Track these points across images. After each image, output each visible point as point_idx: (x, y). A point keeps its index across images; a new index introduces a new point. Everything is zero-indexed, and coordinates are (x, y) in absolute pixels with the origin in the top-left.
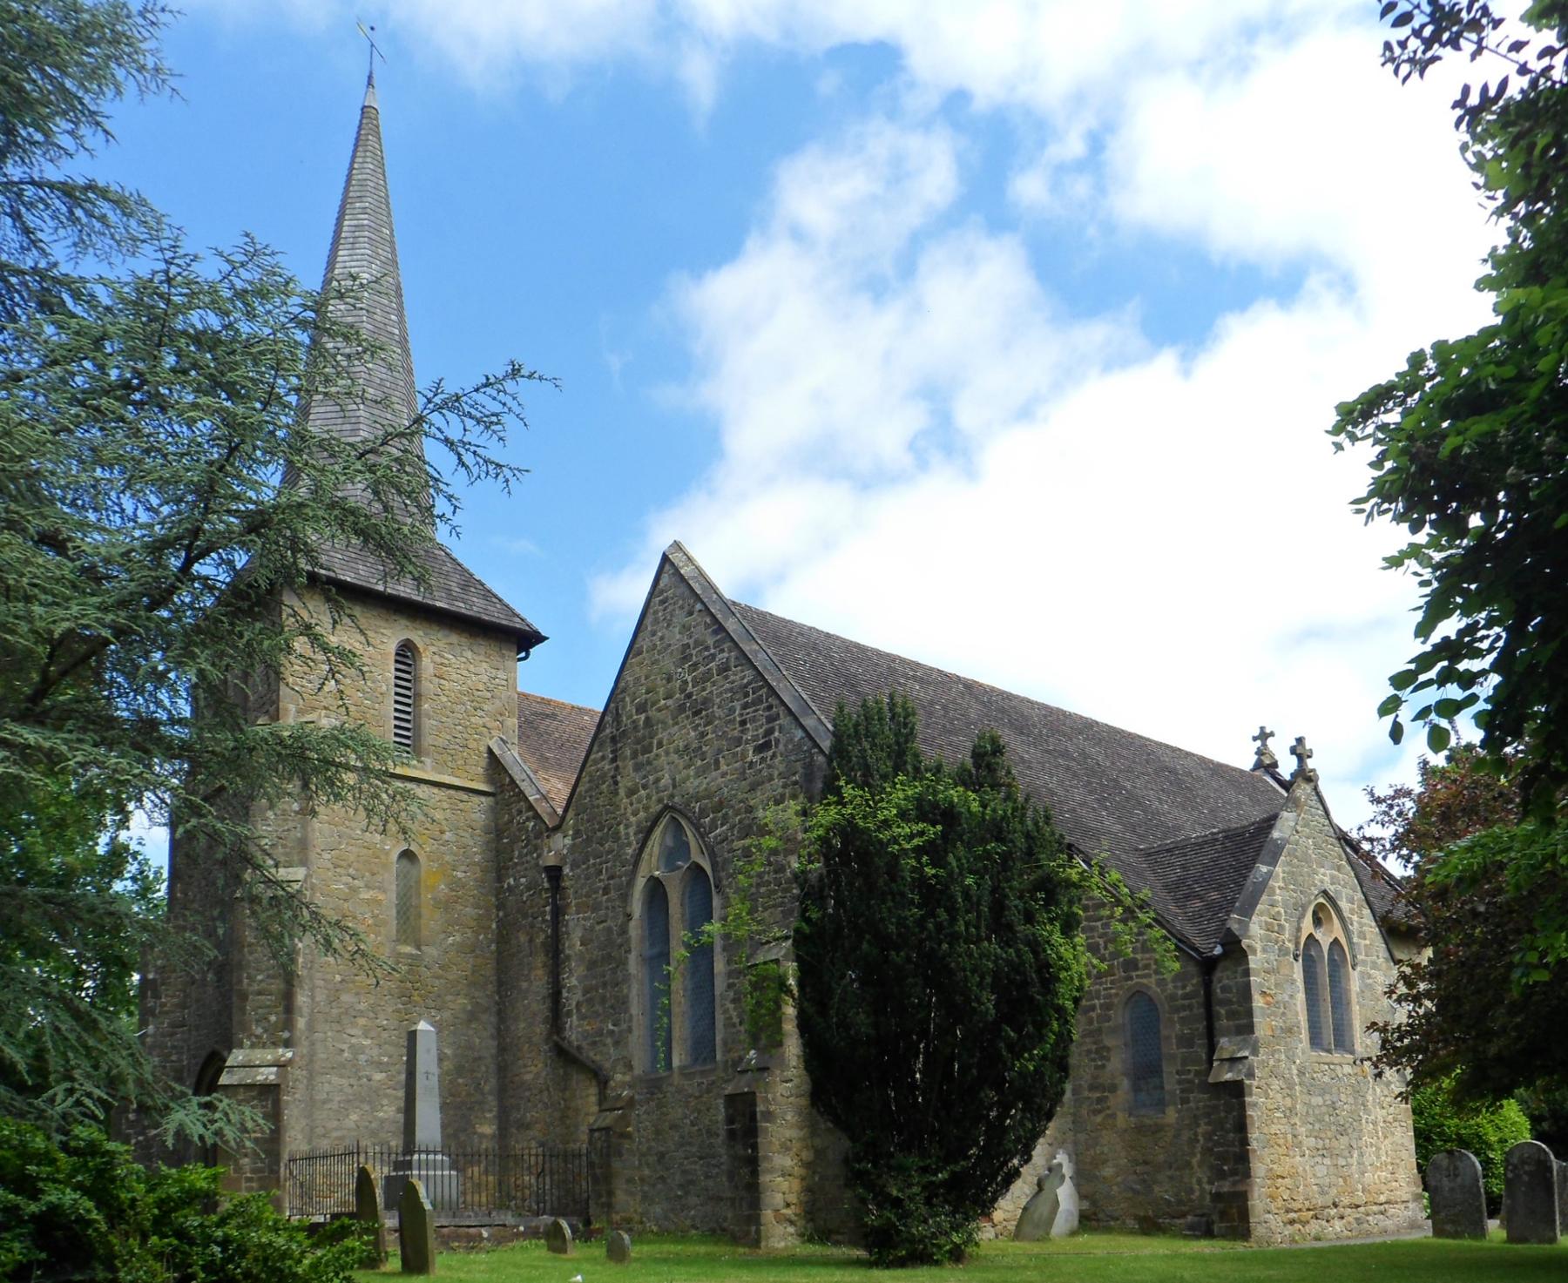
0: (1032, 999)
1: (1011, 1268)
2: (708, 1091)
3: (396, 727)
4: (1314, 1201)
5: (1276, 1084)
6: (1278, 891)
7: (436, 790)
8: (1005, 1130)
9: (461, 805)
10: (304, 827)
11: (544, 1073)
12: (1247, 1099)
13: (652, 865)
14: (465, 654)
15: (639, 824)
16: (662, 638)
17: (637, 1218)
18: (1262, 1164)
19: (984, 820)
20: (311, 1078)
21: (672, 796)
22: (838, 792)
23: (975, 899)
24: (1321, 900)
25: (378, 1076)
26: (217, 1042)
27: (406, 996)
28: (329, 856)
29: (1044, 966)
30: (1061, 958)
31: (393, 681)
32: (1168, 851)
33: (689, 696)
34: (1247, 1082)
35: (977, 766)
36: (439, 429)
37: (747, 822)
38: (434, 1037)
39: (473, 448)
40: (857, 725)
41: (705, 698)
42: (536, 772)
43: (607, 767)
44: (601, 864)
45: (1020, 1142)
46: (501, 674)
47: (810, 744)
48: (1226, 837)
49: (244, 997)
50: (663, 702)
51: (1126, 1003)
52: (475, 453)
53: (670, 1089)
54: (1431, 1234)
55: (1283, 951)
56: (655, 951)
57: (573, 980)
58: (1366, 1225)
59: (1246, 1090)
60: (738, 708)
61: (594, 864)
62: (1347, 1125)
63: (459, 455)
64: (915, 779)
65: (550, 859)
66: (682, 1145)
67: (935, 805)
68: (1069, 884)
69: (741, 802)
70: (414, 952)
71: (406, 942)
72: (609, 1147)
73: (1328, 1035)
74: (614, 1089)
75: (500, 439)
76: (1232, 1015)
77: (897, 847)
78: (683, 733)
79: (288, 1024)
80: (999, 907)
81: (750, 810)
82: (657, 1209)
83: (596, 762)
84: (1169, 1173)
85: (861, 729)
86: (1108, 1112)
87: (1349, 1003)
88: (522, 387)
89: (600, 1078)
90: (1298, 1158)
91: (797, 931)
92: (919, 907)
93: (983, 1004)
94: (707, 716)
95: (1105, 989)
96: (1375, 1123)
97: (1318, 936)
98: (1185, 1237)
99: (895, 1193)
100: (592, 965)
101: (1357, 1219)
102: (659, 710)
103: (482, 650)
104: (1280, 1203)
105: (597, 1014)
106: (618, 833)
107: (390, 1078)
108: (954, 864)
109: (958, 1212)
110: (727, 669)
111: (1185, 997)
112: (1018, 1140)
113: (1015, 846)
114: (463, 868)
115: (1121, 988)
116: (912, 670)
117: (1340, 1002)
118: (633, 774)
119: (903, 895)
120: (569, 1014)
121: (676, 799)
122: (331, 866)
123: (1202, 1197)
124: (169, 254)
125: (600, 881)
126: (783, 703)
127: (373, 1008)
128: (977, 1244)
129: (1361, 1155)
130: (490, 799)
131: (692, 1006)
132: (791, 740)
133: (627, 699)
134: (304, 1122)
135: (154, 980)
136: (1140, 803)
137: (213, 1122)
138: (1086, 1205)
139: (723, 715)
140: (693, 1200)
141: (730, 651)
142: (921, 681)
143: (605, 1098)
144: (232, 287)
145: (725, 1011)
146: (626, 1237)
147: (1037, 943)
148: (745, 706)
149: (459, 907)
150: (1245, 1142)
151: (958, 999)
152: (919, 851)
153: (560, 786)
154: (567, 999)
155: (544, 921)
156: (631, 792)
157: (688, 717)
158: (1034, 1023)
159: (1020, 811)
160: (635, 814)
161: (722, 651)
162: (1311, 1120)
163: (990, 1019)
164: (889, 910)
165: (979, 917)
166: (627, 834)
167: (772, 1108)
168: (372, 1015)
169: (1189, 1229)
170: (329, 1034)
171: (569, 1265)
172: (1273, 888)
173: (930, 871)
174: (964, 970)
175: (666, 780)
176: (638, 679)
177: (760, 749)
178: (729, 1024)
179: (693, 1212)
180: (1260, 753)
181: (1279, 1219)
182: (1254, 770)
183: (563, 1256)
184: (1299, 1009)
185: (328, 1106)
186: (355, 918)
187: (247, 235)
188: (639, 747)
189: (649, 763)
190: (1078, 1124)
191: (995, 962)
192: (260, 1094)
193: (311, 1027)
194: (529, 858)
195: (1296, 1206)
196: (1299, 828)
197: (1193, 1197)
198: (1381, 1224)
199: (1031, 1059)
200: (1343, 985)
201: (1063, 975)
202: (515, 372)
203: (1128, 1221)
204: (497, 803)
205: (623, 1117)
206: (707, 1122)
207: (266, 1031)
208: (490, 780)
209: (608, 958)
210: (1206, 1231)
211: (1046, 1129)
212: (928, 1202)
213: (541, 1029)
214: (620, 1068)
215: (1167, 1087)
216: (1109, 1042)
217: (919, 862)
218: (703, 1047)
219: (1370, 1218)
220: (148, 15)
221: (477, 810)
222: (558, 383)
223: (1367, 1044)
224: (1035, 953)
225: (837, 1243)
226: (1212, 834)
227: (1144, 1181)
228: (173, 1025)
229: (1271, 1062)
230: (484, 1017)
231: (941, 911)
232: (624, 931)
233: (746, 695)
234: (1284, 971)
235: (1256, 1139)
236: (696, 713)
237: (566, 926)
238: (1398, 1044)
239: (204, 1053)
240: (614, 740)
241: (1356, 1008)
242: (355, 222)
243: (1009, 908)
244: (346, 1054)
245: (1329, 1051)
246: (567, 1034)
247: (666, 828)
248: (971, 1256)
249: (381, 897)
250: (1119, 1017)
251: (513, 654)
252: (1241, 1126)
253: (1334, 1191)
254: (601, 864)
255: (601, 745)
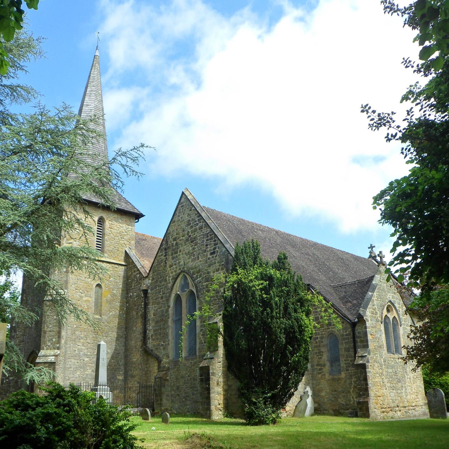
0: (296, 337)
1: (291, 426)
2: (194, 365)
3: (97, 244)
4: (390, 405)
5: (376, 365)
6: (375, 301)
7: (108, 264)
8: (289, 380)
9: (116, 269)
10: (67, 277)
11: (140, 359)
12: (367, 370)
13: (177, 290)
14: (119, 221)
15: (173, 276)
16: (181, 218)
17: (170, 409)
18: (372, 392)
19: (281, 280)
20: (65, 360)
21: (184, 268)
22: (236, 270)
23: (279, 305)
24: (389, 304)
25: (86, 359)
26: (34, 348)
27: (96, 333)
28: (74, 286)
29: (300, 326)
30: (305, 324)
31: (96, 229)
32: (340, 286)
33: (190, 236)
34: (367, 364)
35: (279, 262)
36: (120, 161)
37: (207, 277)
38: (106, 345)
39: (129, 167)
40: (242, 249)
41: (195, 237)
42: (140, 258)
43: (163, 258)
44: (160, 289)
45: (294, 384)
46: (130, 227)
47: (227, 252)
48: (358, 283)
49: (45, 332)
50: (181, 238)
51: (328, 337)
52: (130, 168)
53: (182, 364)
54: (429, 417)
55: (377, 321)
56: (178, 318)
57: (151, 327)
58: (408, 414)
59: (367, 367)
60: (205, 240)
61: (158, 289)
62: (401, 379)
63: (125, 169)
64: (260, 267)
65: (144, 287)
66: (185, 383)
67: (266, 275)
68: (307, 300)
69: (206, 270)
70: (100, 317)
71: (97, 314)
72: (161, 384)
73: (393, 349)
74: (163, 364)
75: (138, 164)
76: (362, 341)
77: (254, 288)
78: (188, 248)
79: (59, 342)
80: (286, 308)
81: (208, 273)
82: (177, 406)
83: (160, 256)
84: (343, 395)
85: (244, 251)
86: (323, 373)
87: (400, 338)
88: (144, 149)
89: (159, 361)
90: (385, 390)
91: (224, 314)
92: (262, 307)
93: (281, 338)
94: (195, 242)
95: (321, 332)
96: (410, 378)
97: (389, 315)
98: (349, 417)
99: (254, 400)
100: (157, 322)
101: (405, 411)
102: (180, 240)
103: (124, 219)
104: (379, 405)
105: (158, 339)
106: (166, 279)
107: (90, 360)
108: (272, 294)
109: (274, 407)
110: (202, 228)
111: (347, 335)
112: (293, 383)
113: (291, 288)
114: (116, 290)
115: (326, 332)
116: (259, 227)
117: (397, 338)
118: (171, 261)
119: (256, 303)
120: (149, 338)
121: (185, 269)
122: (74, 289)
123: (354, 403)
124: (42, 110)
125: (160, 295)
126: (219, 239)
127: (86, 337)
128: (280, 418)
129: (406, 389)
130: (126, 267)
131: (189, 336)
132: (222, 251)
133: (170, 236)
134: (62, 375)
135: (15, 326)
136: (331, 270)
137: (41, 375)
138: (316, 405)
139: (200, 243)
140: (188, 402)
141: (203, 222)
142: (262, 231)
143: (160, 368)
144: (59, 117)
145: (200, 338)
146: (168, 414)
147: (298, 319)
148: (207, 240)
149: (114, 303)
150: (367, 384)
151: (274, 337)
152: (261, 290)
153: (147, 263)
154: (148, 333)
155: (141, 307)
156: (171, 266)
157: (189, 243)
158: (297, 345)
159: (292, 277)
160: (172, 273)
161: (200, 222)
162: (388, 377)
163: (284, 343)
164: (252, 308)
165: (280, 311)
166: (169, 280)
167: (215, 371)
168: (85, 339)
169: (350, 414)
170: (71, 345)
171: (150, 424)
172: (373, 300)
173: (265, 296)
174: (275, 327)
175: (182, 263)
176: (174, 230)
177: (212, 254)
178: (201, 343)
179: (188, 407)
180: (370, 252)
181: (379, 411)
182: (369, 258)
183: (147, 421)
184: (383, 340)
185: (70, 370)
186: (81, 306)
187: (63, 103)
188: (174, 252)
189: (177, 257)
190: (313, 378)
191: (285, 325)
192: (49, 366)
193: (66, 343)
194: (137, 286)
195: (385, 406)
196: (381, 280)
197: (351, 403)
198: (414, 413)
199: (297, 357)
200: (397, 332)
201: (306, 329)
202: (142, 146)
203: (330, 411)
204: (127, 268)
205: (166, 373)
206: (193, 376)
207: (52, 344)
208: (125, 261)
209: (162, 320)
210: (355, 415)
211: (302, 379)
212: (265, 403)
213: (139, 344)
214: (165, 357)
215: (342, 365)
216: (323, 349)
217: (261, 293)
218: (192, 351)
219: (410, 411)
220: (39, 40)
221: (121, 271)
222: (155, 148)
223: (404, 352)
224: (298, 322)
225: (235, 418)
226: (354, 281)
227: (335, 397)
228: (20, 342)
229: (375, 358)
230: (121, 339)
231: (268, 309)
232: (167, 311)
233: (208, 237)
234: (378, 327)
235: (371, 384)
236: (192, 242)
237: (149, 309)
238: (412, 353)
239: (30, 351)
240: (165, 249)
241: (402, 339)
242: (91, 89)
243: (289, 308)
244: (76, 352)
245: (393, 354)
246: (148, 345)
247: (182, 278)
248: (278, 422)
249: (90, 299)
250: (326, 341)
251: (134, 221)
252: (365, 379)
253: (397, 402)
254: (160, 289)
255: (162, 251)
